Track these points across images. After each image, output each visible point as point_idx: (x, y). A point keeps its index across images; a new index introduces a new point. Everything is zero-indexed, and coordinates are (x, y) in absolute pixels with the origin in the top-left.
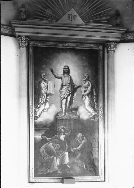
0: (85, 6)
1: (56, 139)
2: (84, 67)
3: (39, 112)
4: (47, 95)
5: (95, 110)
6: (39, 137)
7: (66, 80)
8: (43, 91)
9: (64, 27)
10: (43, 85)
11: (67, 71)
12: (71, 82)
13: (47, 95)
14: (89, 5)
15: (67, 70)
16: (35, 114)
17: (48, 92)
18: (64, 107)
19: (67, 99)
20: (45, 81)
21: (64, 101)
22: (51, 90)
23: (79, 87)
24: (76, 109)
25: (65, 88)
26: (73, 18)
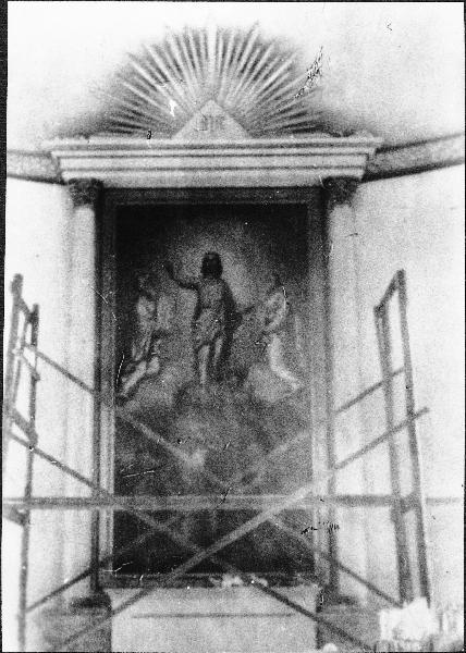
0: (112, 157)
1: (184, 524)
2: (102, 114)
3: (130, 383)
4: (155, 337)
5: (300, 374)
6: (128, 457)
7: (212, 292)
8: (145, 325)
9: (202, 147)
10: (142, 308)
11: (213, 268)
12: (227, 299)
13: (155, 337)
14: (257, 88)
15: (215, 262)
16: (117, 391)
17: (157, 328)
18: (203, 367)
19: (212, 344)
20: (149, 297)
21: (206, 350)
22: (164, 323)
23: (249, 310)
24: (242, 375)
25: (207, 314)
26: (286, 102)
